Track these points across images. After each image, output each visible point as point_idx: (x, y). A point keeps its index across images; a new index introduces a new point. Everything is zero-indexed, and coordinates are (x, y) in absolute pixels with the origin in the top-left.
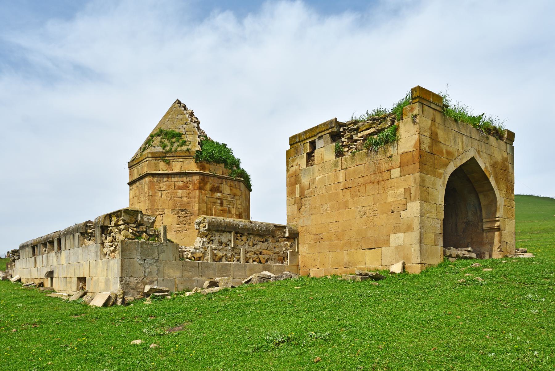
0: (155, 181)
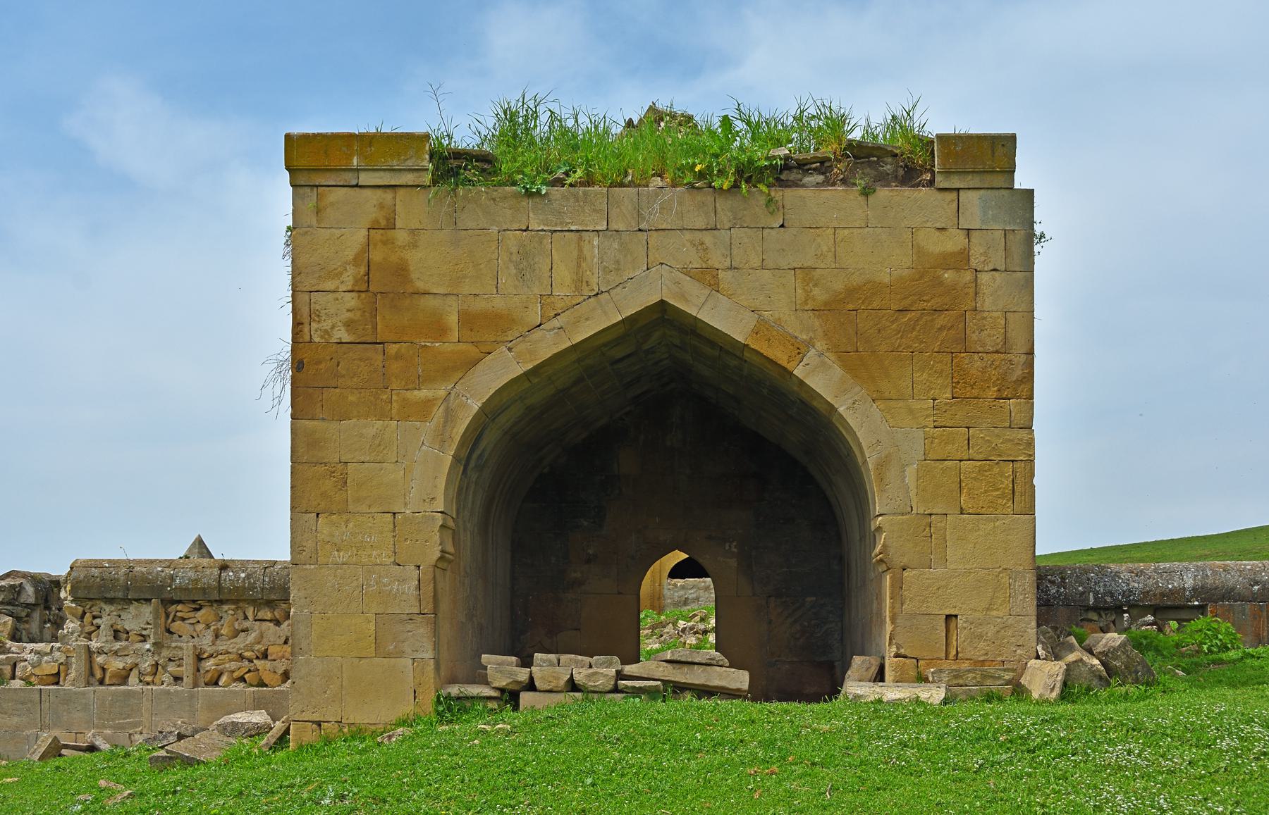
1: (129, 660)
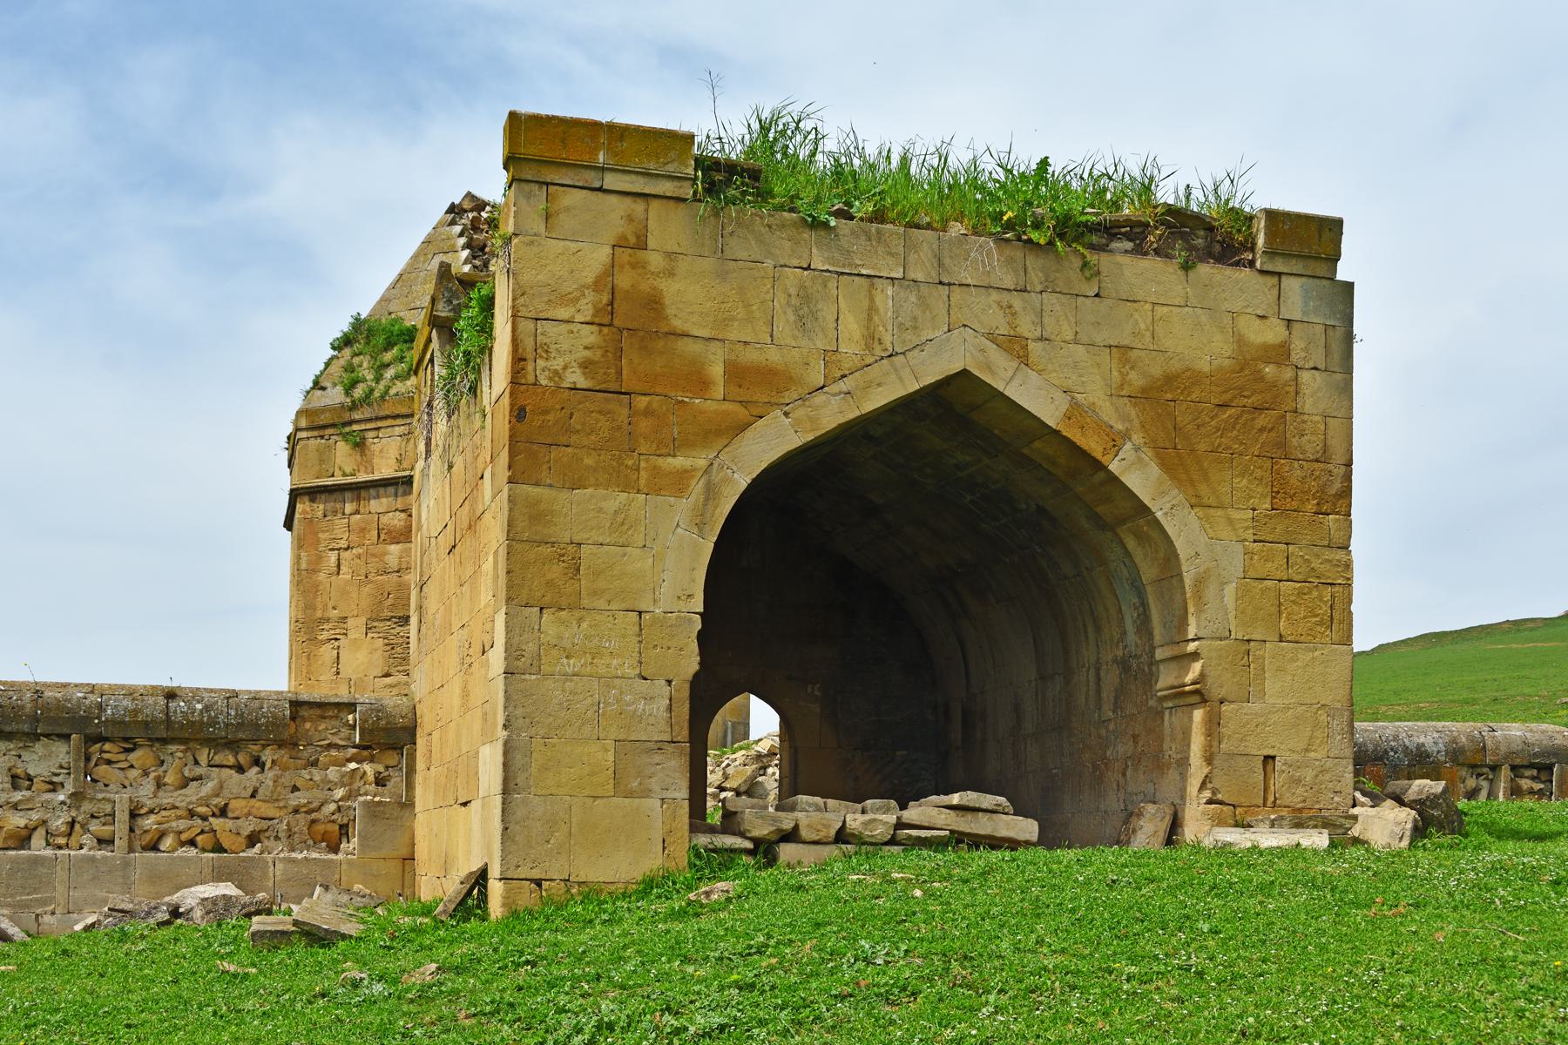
0: (320, 514)
1: (35, 816)
